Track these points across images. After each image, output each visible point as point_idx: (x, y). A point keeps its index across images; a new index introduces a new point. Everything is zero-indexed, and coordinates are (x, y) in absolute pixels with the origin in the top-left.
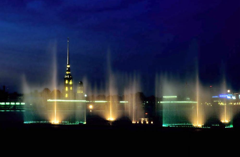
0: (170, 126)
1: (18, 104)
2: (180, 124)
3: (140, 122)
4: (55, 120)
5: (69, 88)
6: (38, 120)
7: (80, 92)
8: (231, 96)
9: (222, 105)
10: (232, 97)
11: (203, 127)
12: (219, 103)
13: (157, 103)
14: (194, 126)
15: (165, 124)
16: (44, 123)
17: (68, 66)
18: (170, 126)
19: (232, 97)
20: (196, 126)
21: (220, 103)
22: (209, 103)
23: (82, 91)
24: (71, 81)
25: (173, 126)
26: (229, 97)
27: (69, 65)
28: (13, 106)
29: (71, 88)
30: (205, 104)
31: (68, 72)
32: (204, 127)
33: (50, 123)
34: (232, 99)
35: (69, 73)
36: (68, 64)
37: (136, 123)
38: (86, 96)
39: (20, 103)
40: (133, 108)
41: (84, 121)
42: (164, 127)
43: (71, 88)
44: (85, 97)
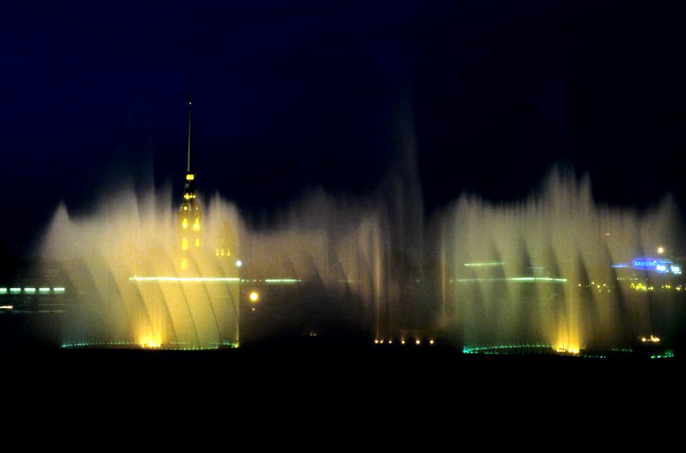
0: (486, 353)
1: (30, 290)
2: (515, 347)
3: (397, 341)
4: (568, 343)
5: (192, 243)
6: (226, 339)
7: (222, 254)
8: (668, 266)
9: (640, 289)
10: (672, 267)
11: (585, 356)
12: (632, 284)
13: (446, 281)
14: (558, 351)
15: (470, 348)
16: (529, 352)
17: (190, 177)
18: (486, 350)
19: (672, 267)
20: (562, 351)
21: (636, 283)
22: (595, 285)
23: (229, 251)
24: (197, 220)
25: (493, 350)
26: (661, 268)
27: (190, 173)
28: (29, 298)
29: (197, 243)
30: (600, 291)
31: (189, 194)
32: (589, 354)
33: (137, 346)
34: (671, 273)
35: (191, 197)
36: (188, 170)
37: (386, 342)
38: (239, 264)
39: (23, 289)
40: (26, 310)
41: (232, 340)
42: (466, 354)
43: (197, 243)
44: (237, 267)
